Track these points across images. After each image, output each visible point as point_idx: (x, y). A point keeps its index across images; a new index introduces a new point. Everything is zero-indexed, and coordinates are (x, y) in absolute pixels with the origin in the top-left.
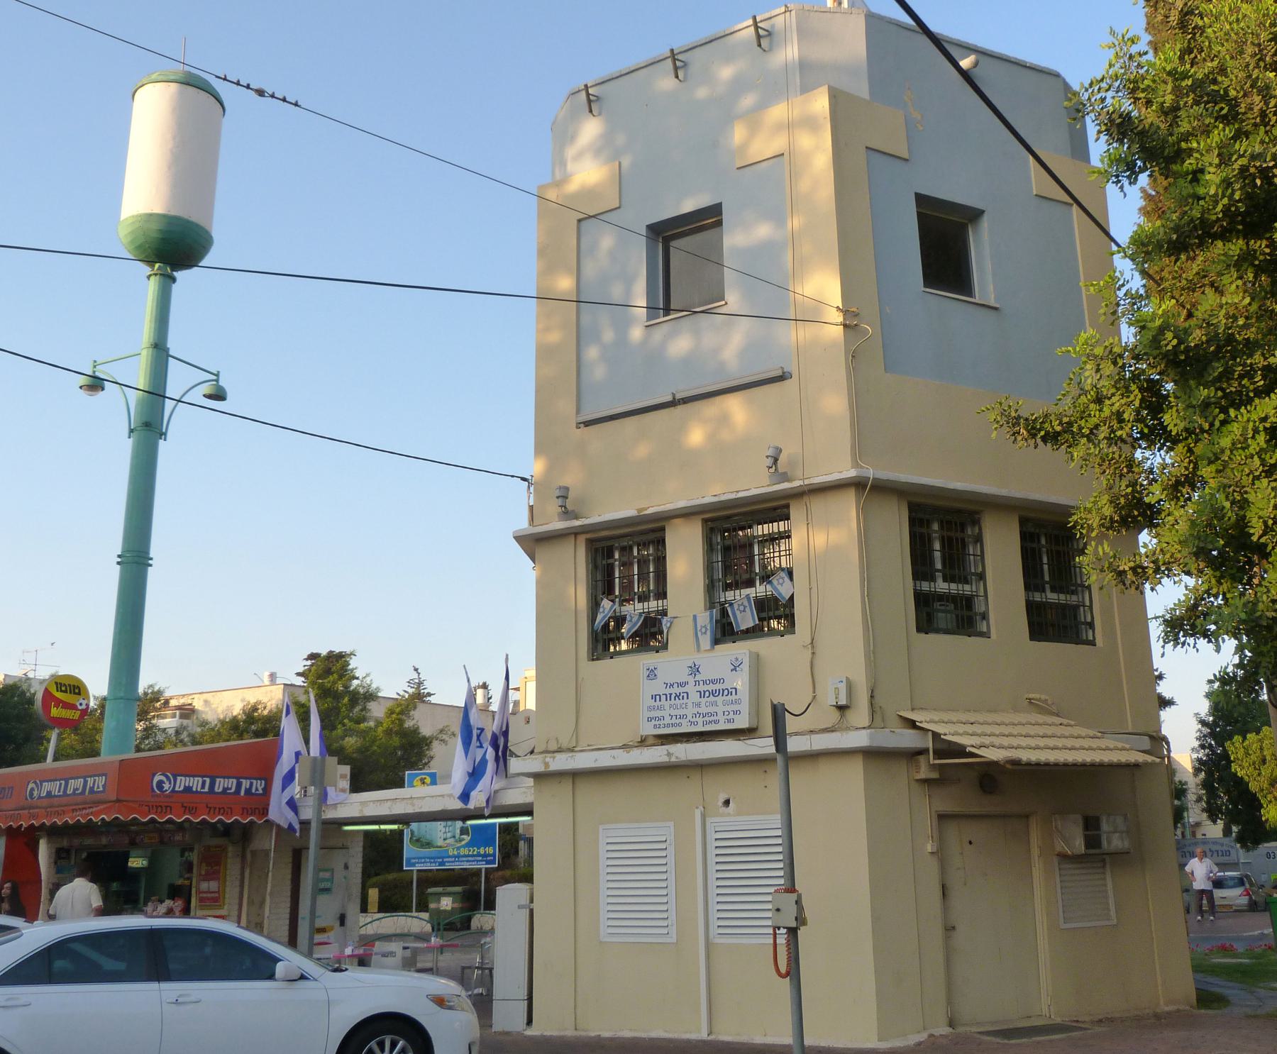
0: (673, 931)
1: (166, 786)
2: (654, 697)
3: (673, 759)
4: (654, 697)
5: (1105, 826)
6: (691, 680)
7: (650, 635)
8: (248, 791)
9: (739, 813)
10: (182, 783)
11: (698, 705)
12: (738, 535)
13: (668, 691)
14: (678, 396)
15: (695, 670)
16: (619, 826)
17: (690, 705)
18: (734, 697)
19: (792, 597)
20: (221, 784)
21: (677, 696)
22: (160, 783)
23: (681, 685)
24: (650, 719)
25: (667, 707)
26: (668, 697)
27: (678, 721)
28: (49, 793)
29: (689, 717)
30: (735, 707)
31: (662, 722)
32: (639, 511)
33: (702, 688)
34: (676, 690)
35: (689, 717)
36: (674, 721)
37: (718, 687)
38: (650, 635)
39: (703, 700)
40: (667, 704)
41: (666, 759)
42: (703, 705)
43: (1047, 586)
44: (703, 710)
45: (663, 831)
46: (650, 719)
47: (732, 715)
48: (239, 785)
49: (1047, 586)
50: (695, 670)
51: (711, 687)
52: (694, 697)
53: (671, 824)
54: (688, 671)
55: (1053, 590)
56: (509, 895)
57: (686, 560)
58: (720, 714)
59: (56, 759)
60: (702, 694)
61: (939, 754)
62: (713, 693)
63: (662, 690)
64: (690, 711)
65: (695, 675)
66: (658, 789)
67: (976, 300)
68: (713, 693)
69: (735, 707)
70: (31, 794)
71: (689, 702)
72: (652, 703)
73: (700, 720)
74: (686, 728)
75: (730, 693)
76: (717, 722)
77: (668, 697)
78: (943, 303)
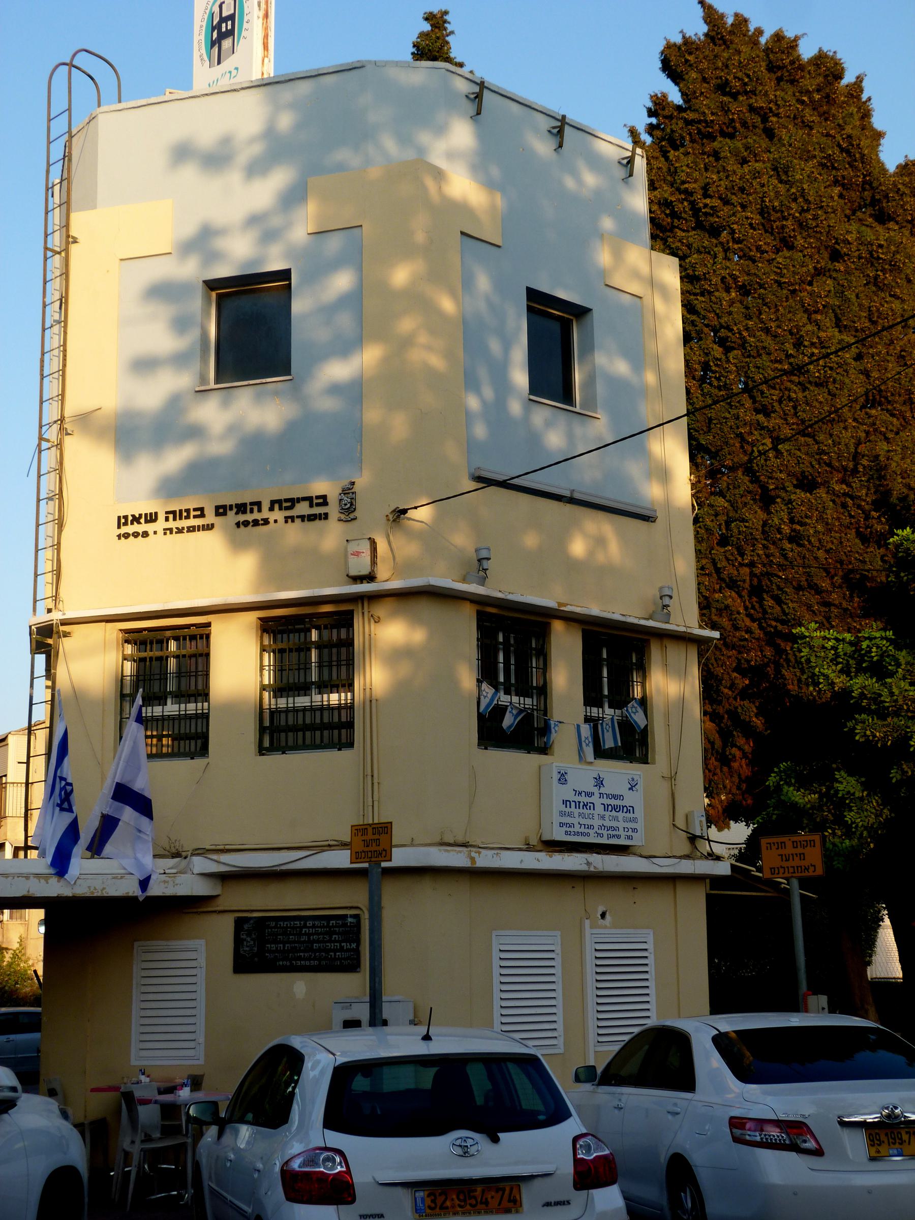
0: (560, 1042)
2: (565, 802)
3: (592, 869)
4: (565, 802)
6: (595, 790)
9: (614, 926)
11: (603, 817)
13: (577, 799)
14: (577, 496)
15: (599, 782)
16: (539, 933)
17: (596, 817)
18: (631, 815)
19: (646, 726)
21: (585, 805)
25: (576, 815)
26: (577, 804)
27: (586, 831)
29: (596, 829)
30: (633, 825)
31: (572, 829)
32: (560, 604)
35: (596, 829)
36: (582, 830)
39: (607, 814)
40: (576, 812)
41: (584, 868)
42: (607, 818)
43: (513, 689)
44: (608, 823)
45: (549, 940)
46: (562, 825)
47: (630, 833)
49: (513, 689)
50: (599, 782)
51: (613, 802)
52: (599, 809)
53: (558, 933)
54: (593, 782)
58: (621, 829)
59: (802, 895)
60: (606, 807)
62: (615, 808)
63: (571, 797)
64: (597, 822)
65: (568, 782)
66: (544, 898)
67: (578, 409)
68: (615, 808)
69: (633, 825)
71: (596, 812)
72: (563, 808)
73: (605, 833)
74: (592, 839)
75: (628, 811)
76: (619, 837)
77: (577, 804)
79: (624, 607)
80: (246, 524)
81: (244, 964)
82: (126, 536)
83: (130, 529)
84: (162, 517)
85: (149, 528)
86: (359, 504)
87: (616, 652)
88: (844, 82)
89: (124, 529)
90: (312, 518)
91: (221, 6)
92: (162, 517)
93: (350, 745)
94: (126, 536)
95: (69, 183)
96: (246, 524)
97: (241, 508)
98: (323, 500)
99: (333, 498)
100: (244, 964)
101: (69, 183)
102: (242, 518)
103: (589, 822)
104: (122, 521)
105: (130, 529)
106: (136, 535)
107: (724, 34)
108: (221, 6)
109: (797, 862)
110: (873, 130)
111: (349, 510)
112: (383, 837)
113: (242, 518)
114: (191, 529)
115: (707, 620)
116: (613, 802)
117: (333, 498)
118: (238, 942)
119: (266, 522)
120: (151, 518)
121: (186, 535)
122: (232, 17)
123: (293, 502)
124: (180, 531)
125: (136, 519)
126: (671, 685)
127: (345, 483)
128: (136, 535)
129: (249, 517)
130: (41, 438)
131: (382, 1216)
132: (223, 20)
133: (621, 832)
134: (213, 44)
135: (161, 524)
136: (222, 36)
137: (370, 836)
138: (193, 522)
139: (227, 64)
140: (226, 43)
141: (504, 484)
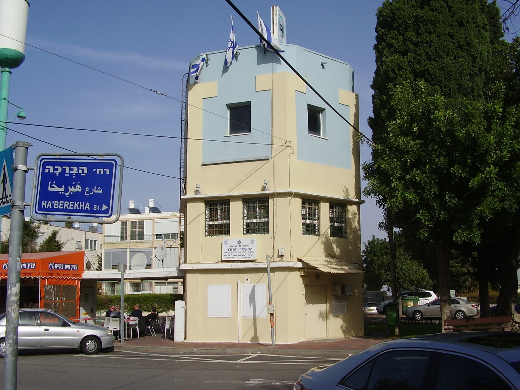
1: (53, 267)
2: (227, 249)
5: (346, 289)
6: (238, 245)
7: (225, 230)
8: (30, 267)
10: (57, 266)
12: (258, 204)
15: (239, 242)
20: (67, 266)
21: (234, 249)
22: (51, 266)
23: (235, 246)
24: (225, 256)
28: (58, 268)
30: (252, 254)
33: (242, 248)
34: (234, 248)
37: (246, 248)
38: (225, 230)
44: (242, 254)
46: (225, 256)
48: (71, 267)
50: (239, 242)
51: (244, 248)
52: (239, 250)
55: (309, 219)
56: (179, 304)
57: (237, 209)
60: (241, 249)
61: (307, 269)
63: (229, 247)
64: (238, 254)
67: (321, 137)
69: (252, 254)
70: (51, 267)
73: (241, 257)
78: (313, 137)
79: (340, 196)
95: (87, 211)
101: (87, 211)
103: (235, 254)
110: (57, 242)
116: (244, 248)
131: (202, 165)
133: (247, 256)
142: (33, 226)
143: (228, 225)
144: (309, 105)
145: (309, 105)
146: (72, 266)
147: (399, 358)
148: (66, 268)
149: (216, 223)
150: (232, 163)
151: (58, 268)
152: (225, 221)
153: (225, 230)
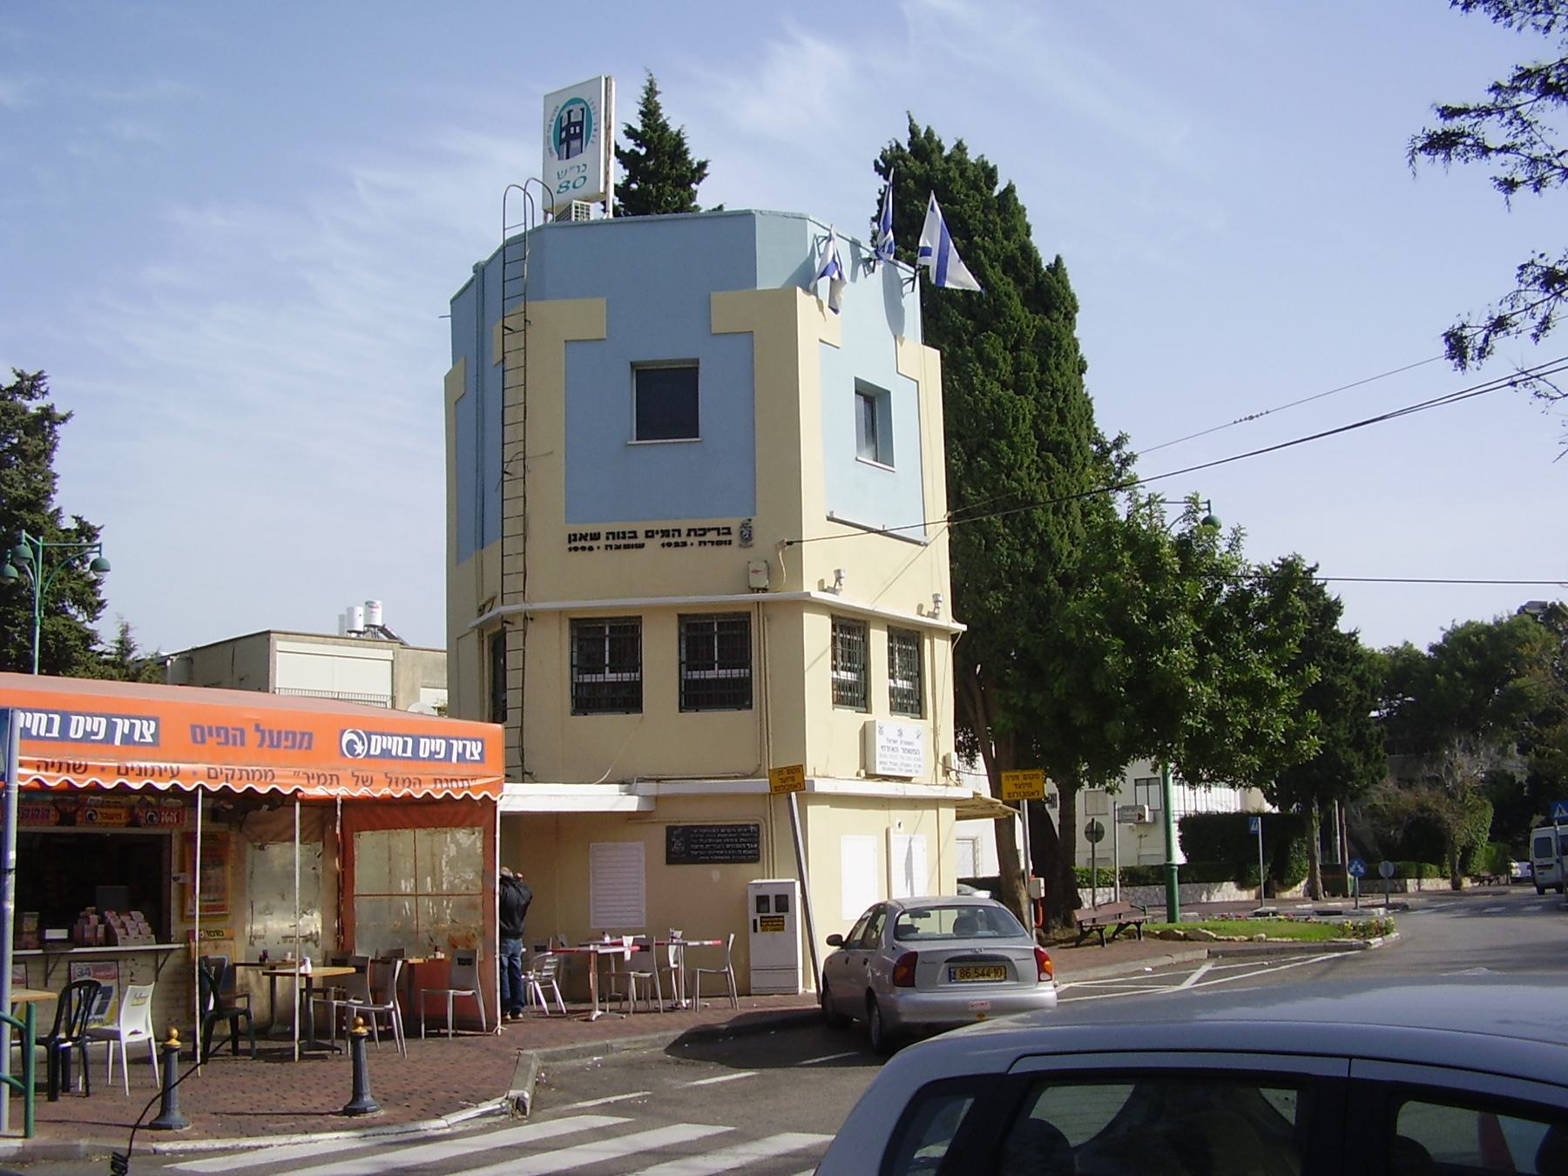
1: (359, 748)
7: (628, 699)
10: (378, 744)
22: (351, 743)
48: (449, 747)
50: (901, 734)
80: (669, 545)
81: (672, 858)
82: (576, 549)
83: (579, 544)
84: (603, 536)
85: (594, 544)
86: (755, 536)
87: (907, 639)
88: (946, 153)
89: (574, 544)
90: (719, 543)
91: (569, 113)
92: (603, 536)
93: (750, 707)
94: (576, 549)
96: (669, 545)
97: (665, 533)
98: (728, 531)
99: (735, 529)
100: (672, 858)
102: (666, 540)
104: (572, 538)
105: (579, 544)
106: (583, 548)
107: (923, 146)
108: (569, 113)
109: (1027, 789)
111: (747, 538)
112: (797, 776)
113: (666, 540)
114: (627, 547)
115: (957, 616)
117: (735, 529)
118: (669, 843)
119: (685, 544)
120: (596, 537)
121: (622, 551)
122: (580, 124)
123: (705, 531)
124: (618, 547)
125: (583, 537)
126: (940, 659)
127: (744, 519)
128: (583, 548)
129: (672, 540)
130: (504, 472)
132: (570, 124)
134: (562, 142)
135: (602, 542)
136: (570, 138)
137: (785, 775)
138: (627, 542)
139: (577, 160)
140: (575, 144)
141: (870, 530)
142: (1123, 518)
143: (637, 687)
144: (633, 365)
145: (633, 365)
146: (457, 746)
147: (211, 1007)
148: (424, 753)
149: (600, 678)
150: (1402, 412)
151: (386, 753)
152: (735, 671)
153: (628, 699)
